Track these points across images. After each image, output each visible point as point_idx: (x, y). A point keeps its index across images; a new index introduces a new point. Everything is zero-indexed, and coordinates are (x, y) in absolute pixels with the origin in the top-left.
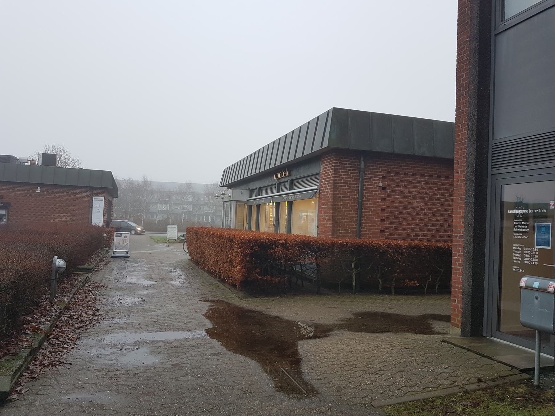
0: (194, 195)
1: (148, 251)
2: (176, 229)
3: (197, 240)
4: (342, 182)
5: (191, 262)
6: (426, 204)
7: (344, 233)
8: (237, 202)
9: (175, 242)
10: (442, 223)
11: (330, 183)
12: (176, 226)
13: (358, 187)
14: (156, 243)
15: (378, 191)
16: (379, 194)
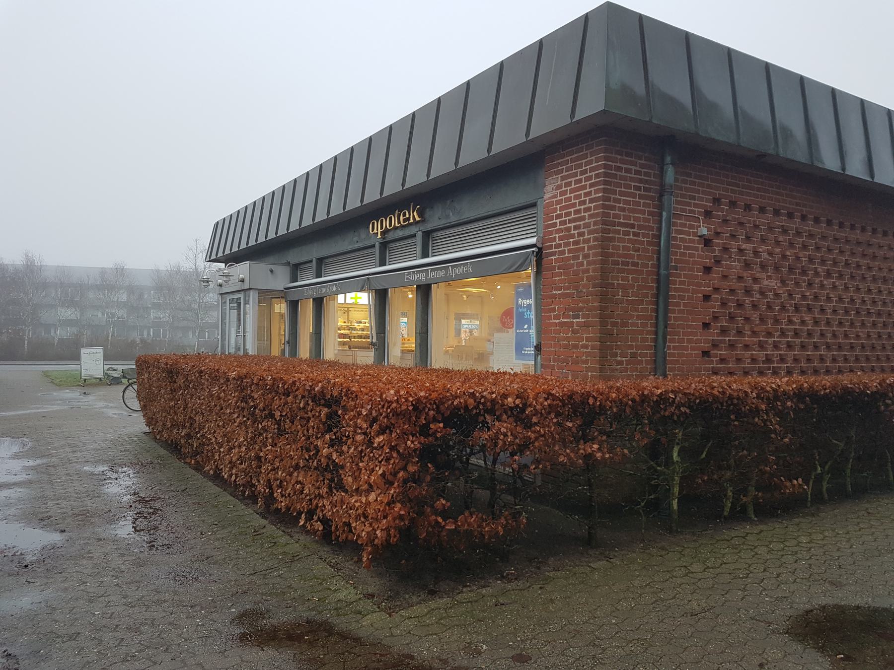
0: (131, 290)
1: (38, 408)
2: (100, 356)
3: (173, 391)
4: (622, 220)
5: (153, 444)
6: (783, 282)
7: (628, 363)
8: (261, 292)
9: (100, 383)
10: (810, 328)
11: (586, 226)
12: (100, 351)
13: (659, 237)
14: (58, 387)
15: (696, 249)
16: (699, 256)
